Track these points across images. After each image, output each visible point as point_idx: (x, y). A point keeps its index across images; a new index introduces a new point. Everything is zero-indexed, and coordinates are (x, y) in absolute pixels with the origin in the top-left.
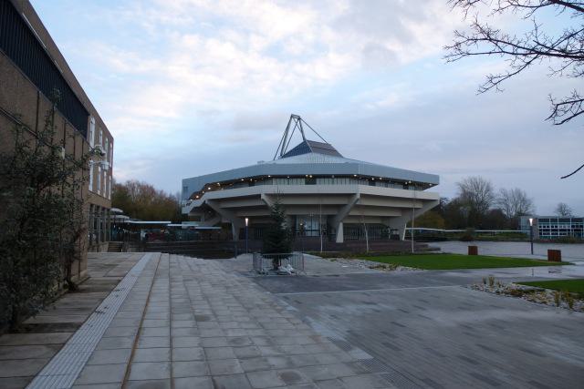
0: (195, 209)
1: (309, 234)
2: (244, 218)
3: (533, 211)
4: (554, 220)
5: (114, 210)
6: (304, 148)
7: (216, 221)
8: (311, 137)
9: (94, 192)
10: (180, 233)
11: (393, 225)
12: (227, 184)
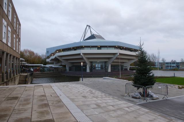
0: (52, 60)
1: (98, 69)
2: (80, 63)
3: (163, 60)
4: (170, 63)
5: (21, 59)
6: (93, 37)
7: (60, 64)
8: (94, 33)
9: (11, 48)
10: (46, 69)
11: (125, 65)
12: (64, 50)
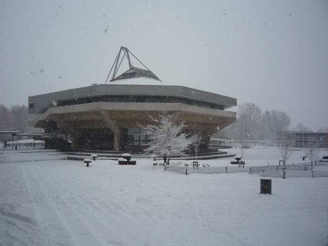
8: (136, 65)
